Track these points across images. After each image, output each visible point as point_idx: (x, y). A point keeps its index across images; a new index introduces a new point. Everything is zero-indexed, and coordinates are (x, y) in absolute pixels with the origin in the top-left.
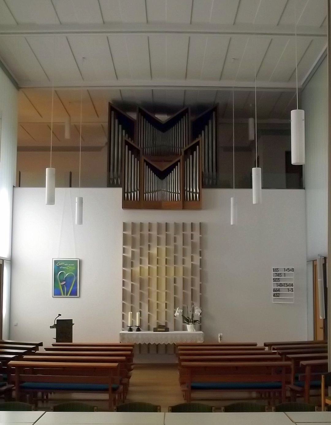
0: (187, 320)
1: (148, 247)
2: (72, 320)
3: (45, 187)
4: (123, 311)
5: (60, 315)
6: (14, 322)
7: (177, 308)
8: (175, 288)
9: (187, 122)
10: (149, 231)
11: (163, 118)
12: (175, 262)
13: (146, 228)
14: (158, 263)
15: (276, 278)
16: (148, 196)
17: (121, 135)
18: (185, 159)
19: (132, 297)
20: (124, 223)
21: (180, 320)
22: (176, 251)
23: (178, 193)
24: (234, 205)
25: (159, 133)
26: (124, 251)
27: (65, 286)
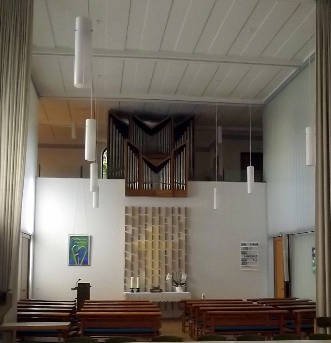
0: (176, 283)
1: (145, 226)
3: (89, 177)
4: (125, 277)
5: (80, 279)
6: (36, 286)
9: (170, 130)
10: (146, 213)
11: (150, 124)
13: (143, 211)
14: (152, 239)
15: (244, 251)
16: (146, 186)
17: (118, 137)
18: (175, 158)
19: (132, 265)
20: (126, 207)
21: (170, 283)
22: (166, 229)
25: (148, 137)
27: (78, 257)
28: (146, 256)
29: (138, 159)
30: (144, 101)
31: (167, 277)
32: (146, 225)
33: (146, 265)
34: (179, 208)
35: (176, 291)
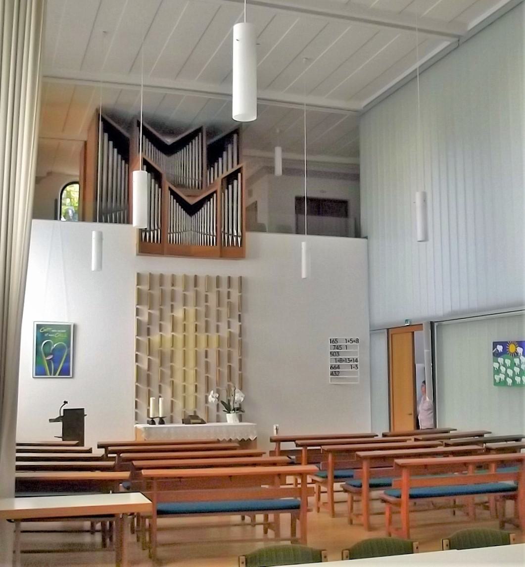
2: (83, 409)
5: (66, 402)
8: (207, 365)
10: (173, 285)
12: (207, 330)
15: (335, 352)
20: (138, 275)
22: (207, 315)
27: (52, 362)
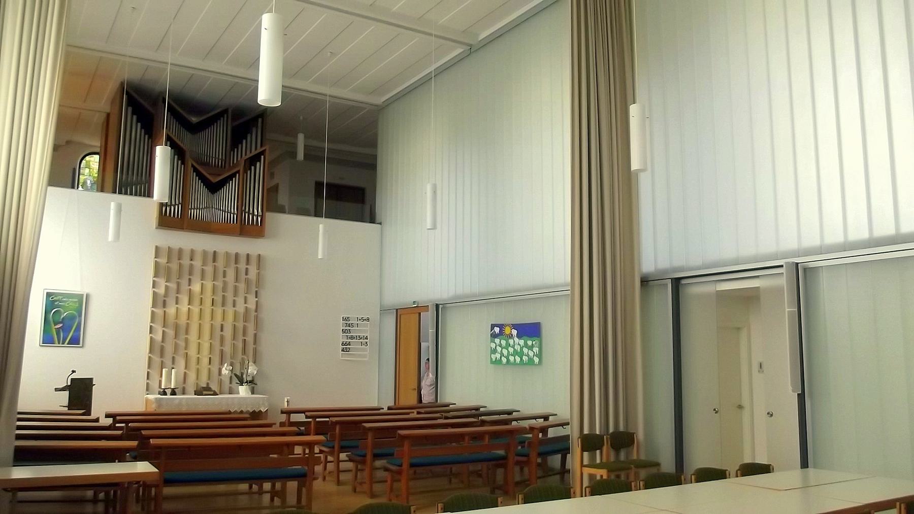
2: (91, 379)
5: (73, 372)
7: (225, 364)
8: (222, 339)
12: (223, 304)
20: (157, 247)
22: (224, 289)
23: (234, 214)
24: (324, 234)
26: (154, 285)
27: (61, 330)
28: (187, 332)
29: (183, 166)
30: (192, 72)
31: (224, 369)
32: (190, 280)
33: (186, 348)
34: (248, 255)
35: (239, 393)
